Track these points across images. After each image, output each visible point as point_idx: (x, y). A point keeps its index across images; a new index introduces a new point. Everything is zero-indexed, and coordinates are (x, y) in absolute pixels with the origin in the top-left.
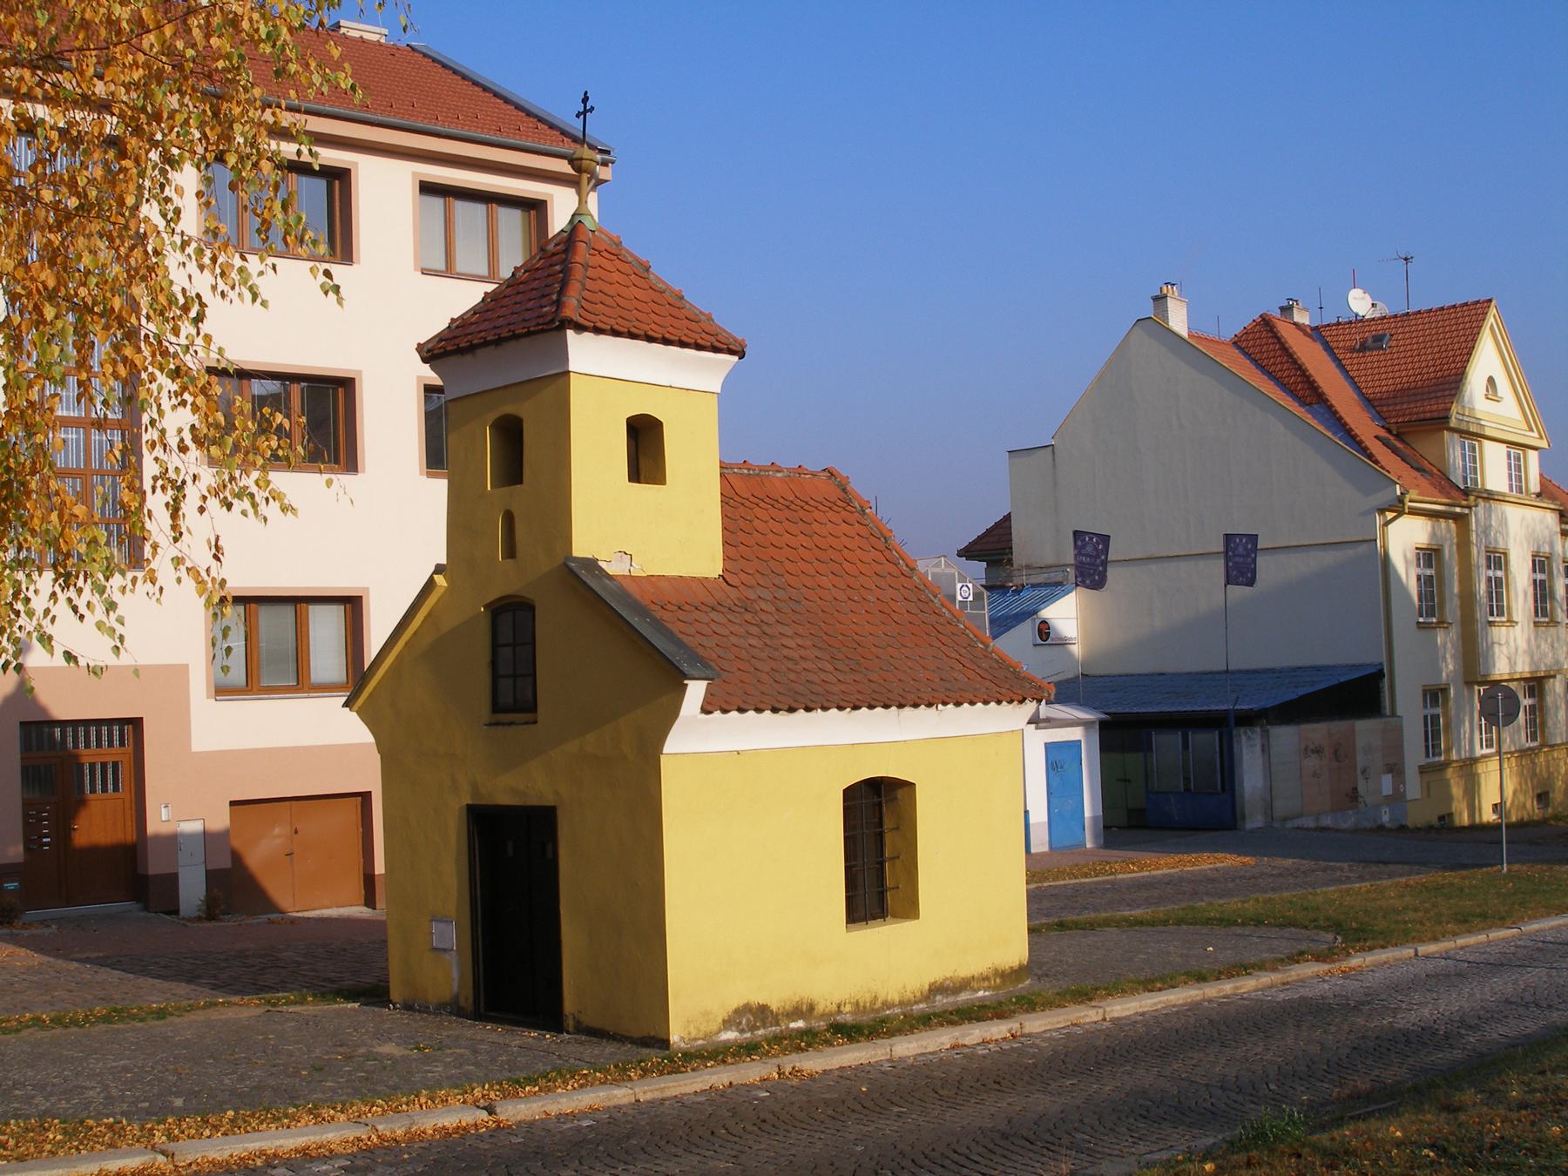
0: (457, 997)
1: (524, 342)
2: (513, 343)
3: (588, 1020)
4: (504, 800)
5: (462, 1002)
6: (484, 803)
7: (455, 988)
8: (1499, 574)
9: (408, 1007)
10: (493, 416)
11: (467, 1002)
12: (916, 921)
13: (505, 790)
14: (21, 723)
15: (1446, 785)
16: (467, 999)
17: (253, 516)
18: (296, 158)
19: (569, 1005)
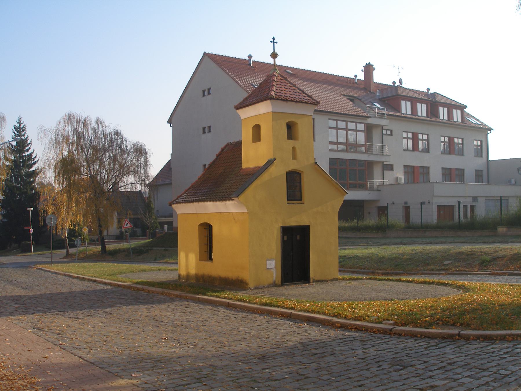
0: (275, 282)
1: (304, 104)
2: (300, 104)
3: (316, 279)
4: (293, 224)
5: (277, 282)
6: (286, 225)
7: (274, 278)
8: (471, 337)
9: (256, 288)
10: (288, 121)
11: (279, 280)
12: (438, 205)
13: (293, 222)
14: (442, 168)
15: (463, 334)
16: (278, 281)
17: (31, 134)
18: (271, 61)
19: (312, 276)
